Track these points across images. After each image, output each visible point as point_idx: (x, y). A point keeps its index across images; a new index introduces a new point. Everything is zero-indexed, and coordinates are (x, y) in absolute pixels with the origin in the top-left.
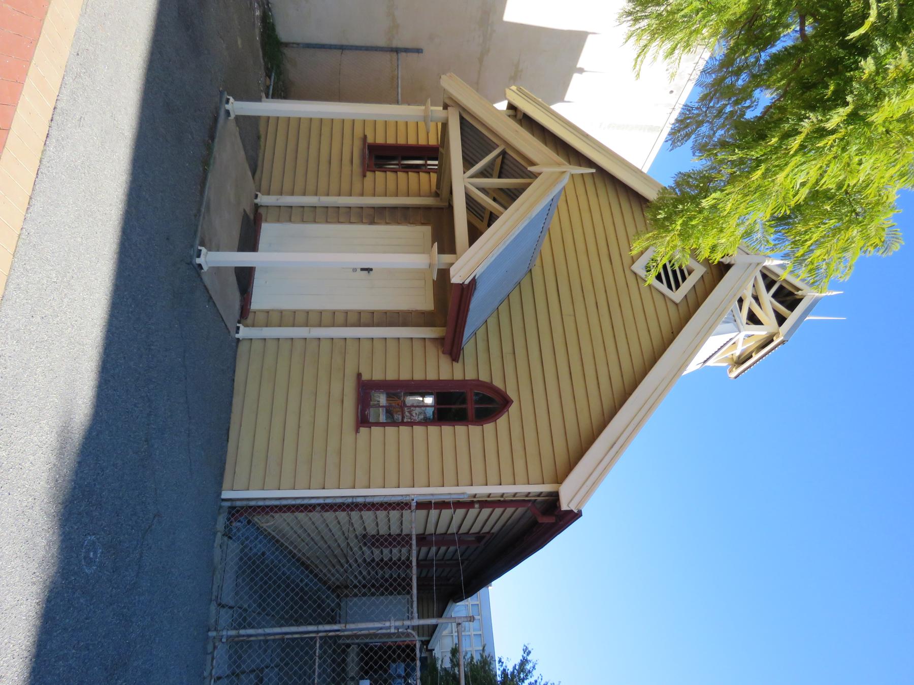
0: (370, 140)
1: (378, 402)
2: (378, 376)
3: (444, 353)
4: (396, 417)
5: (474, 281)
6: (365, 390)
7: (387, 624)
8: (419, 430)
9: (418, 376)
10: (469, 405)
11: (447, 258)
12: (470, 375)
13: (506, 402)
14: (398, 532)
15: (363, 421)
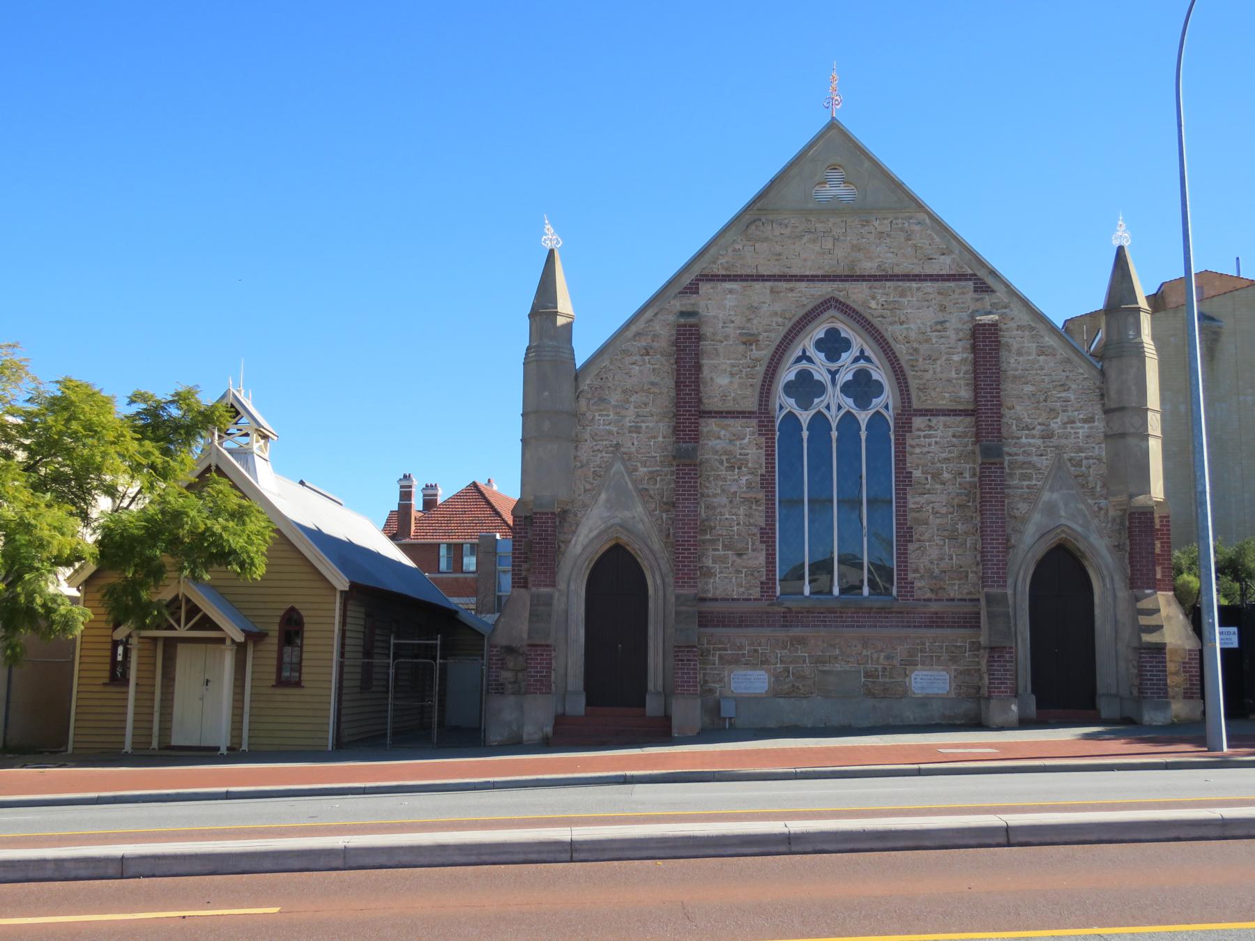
0: (107, 681)
1: (288, 679)
2: (274, 676)
4: (298, 667)
5: (243, 630)
6: (281, 683)
8: (305, 656)
9: (275, 655)
10: (292, 628)
11: (228, 642)
12: (277, 627)
13: (292, 609)
15: (298, 684)
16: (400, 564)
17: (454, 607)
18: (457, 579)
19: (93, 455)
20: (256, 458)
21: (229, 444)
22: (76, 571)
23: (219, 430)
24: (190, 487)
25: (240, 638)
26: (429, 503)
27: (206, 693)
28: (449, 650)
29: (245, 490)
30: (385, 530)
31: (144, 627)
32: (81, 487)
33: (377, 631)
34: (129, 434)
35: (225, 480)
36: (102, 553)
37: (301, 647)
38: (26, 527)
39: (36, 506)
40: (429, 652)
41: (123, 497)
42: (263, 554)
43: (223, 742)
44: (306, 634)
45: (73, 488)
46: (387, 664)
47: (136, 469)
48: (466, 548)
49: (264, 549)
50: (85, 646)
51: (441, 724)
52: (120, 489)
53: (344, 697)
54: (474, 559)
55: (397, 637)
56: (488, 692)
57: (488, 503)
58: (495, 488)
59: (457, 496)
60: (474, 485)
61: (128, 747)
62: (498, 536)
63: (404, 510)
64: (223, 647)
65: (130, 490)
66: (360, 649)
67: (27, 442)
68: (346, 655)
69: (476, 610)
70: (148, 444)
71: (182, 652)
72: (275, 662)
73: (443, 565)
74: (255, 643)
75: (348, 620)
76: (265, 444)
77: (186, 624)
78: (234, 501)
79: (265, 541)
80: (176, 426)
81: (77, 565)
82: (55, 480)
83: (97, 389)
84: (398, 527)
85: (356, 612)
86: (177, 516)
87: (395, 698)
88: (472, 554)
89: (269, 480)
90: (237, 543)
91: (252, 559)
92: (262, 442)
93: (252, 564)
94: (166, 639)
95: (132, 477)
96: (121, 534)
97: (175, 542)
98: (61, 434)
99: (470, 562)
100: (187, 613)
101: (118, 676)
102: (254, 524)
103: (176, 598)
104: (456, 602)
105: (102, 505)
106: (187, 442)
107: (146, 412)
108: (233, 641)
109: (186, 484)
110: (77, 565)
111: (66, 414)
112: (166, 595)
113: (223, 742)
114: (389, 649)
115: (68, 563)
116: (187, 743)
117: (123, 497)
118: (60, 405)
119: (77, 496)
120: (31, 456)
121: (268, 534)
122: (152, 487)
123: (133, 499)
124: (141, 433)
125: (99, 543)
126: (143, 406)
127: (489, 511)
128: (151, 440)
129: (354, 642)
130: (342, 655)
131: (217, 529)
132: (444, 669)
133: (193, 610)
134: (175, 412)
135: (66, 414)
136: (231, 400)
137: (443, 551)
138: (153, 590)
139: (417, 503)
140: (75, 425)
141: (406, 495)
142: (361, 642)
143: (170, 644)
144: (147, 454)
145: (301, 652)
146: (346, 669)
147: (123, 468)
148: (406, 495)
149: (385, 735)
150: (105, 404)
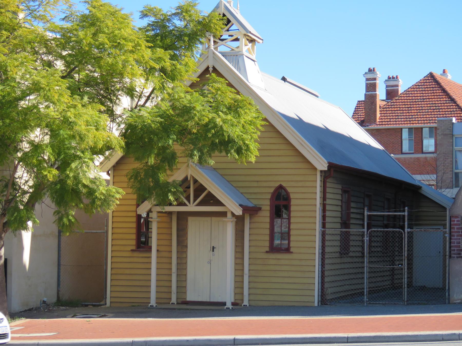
1: (279, 246)
2: (267, 244)
3: (257, 214)
4: (287, 235)
5: (240, 205)
6: (273, 249)
7: (366, 241)
8: (292, 226)
9: (268, 226)
10: (281, 203)
11: (229, 215)
12: (268, 202)
13: (281, 187)
14: (339, 236)
15: (287, 250)
16: (369, 146)
17: (417, 183)
18: (418, 159)
19: (117, 63)
20: (246, 59)
21: (222, 48)
22: (106, 158)
23: (214, 37)
24: (192, 86)
25: (239, 212)
26: (391, 93)
27: (213, 257)
28: (415, 220)
29: (236, 86)
30: (355, 116)
31: (165, 202)
32: (107, 89)
33: (353, 205)
34: (144, 44)
35: (222, 80)
36: (127, 144)
37: (289, 219)
38: (67, 122)
39: (75, 107)
40: (397, 222)
41: (141, 96)
42: (256, 141)
43: (229, 299)
44: (292, 208)
45: (103, 91)
46: (361, 233)
47: (149, 72)
48: (426, 131)
49: (255, 136)
50: (115, 219)
51: (410, 285)
52: (138, 89)
53: (327, 261)
54: (432, 141)
55: (369, 210)
56: (450, 257)
57: (444, 91)
58: (450, 77)
59: (417, 86)
60: (431, 75)
61: (153, 302)
62: (454, 120)
63: (370, 99)
64: (224, 219)
65: (145, 91)
66: (339, 220)
67: (64, 53)
68: (327, 225)
69: (437, 186)
70: (160, 52)
71: (192, 223)
72: (268, 232)
73: (406, 147)
74: (251, 216)
75: (328, 196)
76: (253, 47)
77: (195, 201)
78: (229, 97)
79: (257, 129)
80: (180, 35)
81: (107, 153)
82: (87, 84)
83: (118, 8)
84: (365, 114)
85: (334, 190)
86: (186, 111)
87: (370, 262)
88: (431, 136)
89: (258, 78)
90: (234, 132)
91: (247, 146)
92: (250, 45)
93: (248, 149)
94: (179, 213)
95: (147, 79)
96: (141, 129)
97: (183, 133)
98: (90, 44)
99: (429, 144)
100: (195, 191)
101: (143, 244)
102: (249, 115)
103: (186, 179)
104: (419, 179)
105: (124, 103)
106: (189, 47)
107: (152, 26)
108: (233, 214)
109: (190, 83)
110: (107, 153)
111: (93, 30)
112: (178, 176)
113: (229, 299)
114: (363, 220)
115: (101, 152)
116: (200, 299)
117: (140, 97)
118: (90, 21)
119: (103, 97)
120: (67, 64)
121: (259, 123)
122: (163, 88)
123: (148, 98)
124: (153, 42)
125: (124, 135)
126: (153, 19)
127: (445, 98)
128: (160, 47)
129: (334, 214)
130: (324, 225)
131: (219, 121)
132: (411, 236)
133: (200, 189)
134: (179, 23)
135: (93, 30)
136: (223, 10)
137: (405, 134)
138: (169, 172)
139: (381, 93)
140: (102, 38)
141: (371, 87)
142: (339, 214)
143: (182, 218)
144: (159, 60)
145: (289, 223)
146: (327, 237)
147: (139, 72)
148: (371, 87)
149: (362, 294)
150: (123, 20)
